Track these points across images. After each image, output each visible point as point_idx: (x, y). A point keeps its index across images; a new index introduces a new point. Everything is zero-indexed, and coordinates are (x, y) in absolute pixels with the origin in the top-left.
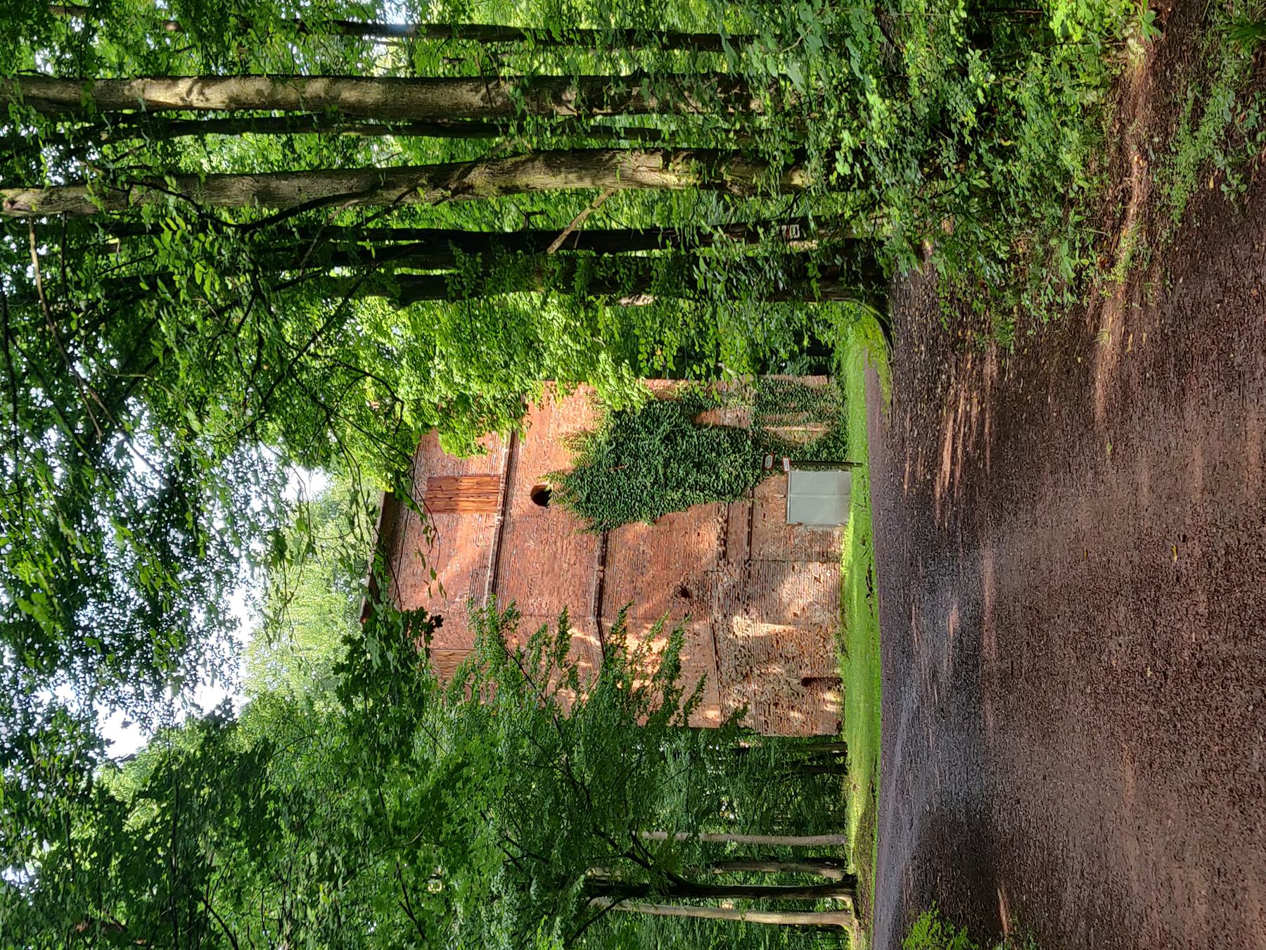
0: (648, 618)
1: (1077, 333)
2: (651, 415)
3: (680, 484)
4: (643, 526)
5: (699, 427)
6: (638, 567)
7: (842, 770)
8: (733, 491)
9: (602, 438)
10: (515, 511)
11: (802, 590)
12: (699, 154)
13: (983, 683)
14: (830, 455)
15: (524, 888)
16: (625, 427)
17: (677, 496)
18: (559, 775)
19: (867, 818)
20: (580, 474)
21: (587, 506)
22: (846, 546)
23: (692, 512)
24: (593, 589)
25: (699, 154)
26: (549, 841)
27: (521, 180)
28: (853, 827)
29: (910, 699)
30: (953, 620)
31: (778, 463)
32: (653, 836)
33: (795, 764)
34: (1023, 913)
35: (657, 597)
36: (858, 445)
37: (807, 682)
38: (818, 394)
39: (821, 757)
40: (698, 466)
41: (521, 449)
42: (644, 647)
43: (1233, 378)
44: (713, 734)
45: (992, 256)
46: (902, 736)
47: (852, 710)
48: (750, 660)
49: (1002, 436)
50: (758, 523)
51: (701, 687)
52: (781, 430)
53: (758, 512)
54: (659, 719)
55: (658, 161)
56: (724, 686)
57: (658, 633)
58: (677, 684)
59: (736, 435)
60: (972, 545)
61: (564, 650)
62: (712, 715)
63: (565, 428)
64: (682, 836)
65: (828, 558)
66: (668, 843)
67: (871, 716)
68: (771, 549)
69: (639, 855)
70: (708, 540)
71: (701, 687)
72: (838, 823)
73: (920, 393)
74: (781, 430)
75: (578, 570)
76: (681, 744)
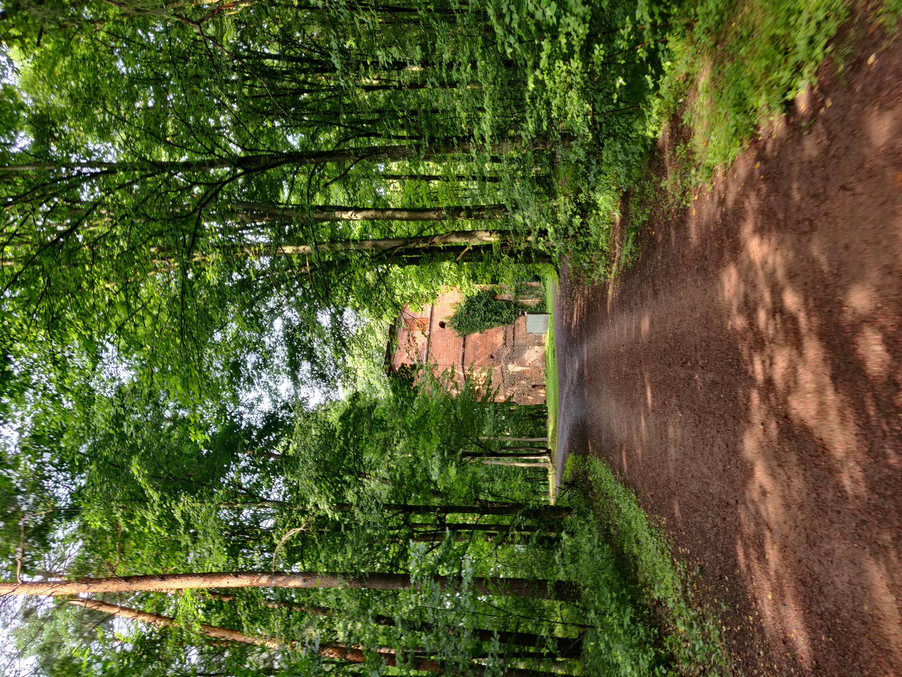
0: (479, 365)
1: (604, 287)
2: (479, 297)
3: (490, 320)
4: (477, 334)
5: (496, 300)
6: (476, 348)
7: (546, 417)
8: (508, 322)
9: (463, 305)
10: (433, 330)
11: (532, 355)
12: (499, 232)
13: (582, 382)
14: (540, 309)
15: (443, 454)
16: (471, 302)
17: (488, 324)
18: (452, 417)
19: (554, 430)
20: (456, 317)
21: (458, 328)
22: (547, 340)
23: (494, 329)
24: (461, 356)
25: (499, 232)
26: (450, 440)
27: (449, 240)
28: (550, 434)
29: (566, 389)
30: (577, 366)
31: (523, 314)
32: (483, 438)
33: (530, 415)
34: (593, 444)
35: (482, 359)
36: (550, 306)
37: (534, 386)
38: (537, 288)
39: (539, 413)
40: (496, 314)
41: (435, 307)
42: (479, 376)
43: (631, 311)
44: (503, 404)
45: (585, 261)
46: (564, 401)
47: (549, 395)
48: (514, 379)
49: (588, 313)
50: (516, 333)
51: (498, 388)
52: (524, 301)
53: (516, 329)
54: (485, 399)
55: (488, 234)
56: (506, 388)
57: (484, 370)
58: (491, 387)
59: (508, 303)
60: (581, 344)
61: (453, 376)
62: (501, 398)
63: (450, 301)
64: (492, 438)
65: (541, 344)
66: (488, 441)
67: (555, 397)
68: (521, 342)
69: (479, 444)
70: (499, 339)
71: (498, 388)
72: (545, 435)
73: (568, 293)
74: (524, 301)
75: (455, 349)
76: (491, 407)
